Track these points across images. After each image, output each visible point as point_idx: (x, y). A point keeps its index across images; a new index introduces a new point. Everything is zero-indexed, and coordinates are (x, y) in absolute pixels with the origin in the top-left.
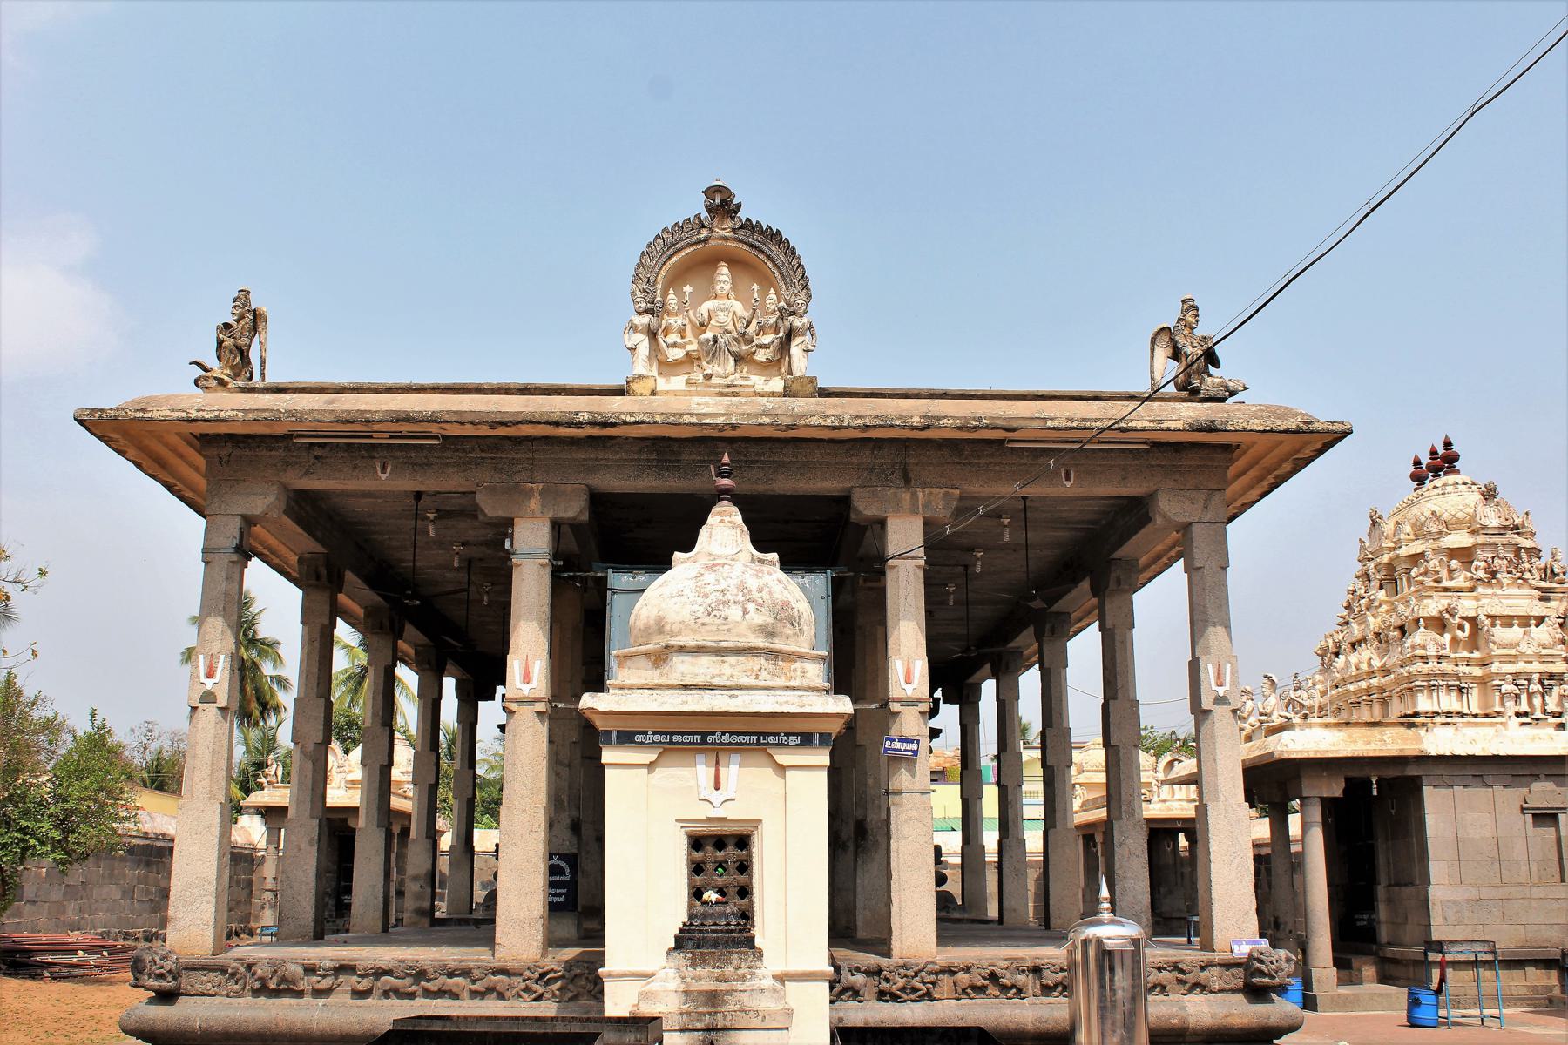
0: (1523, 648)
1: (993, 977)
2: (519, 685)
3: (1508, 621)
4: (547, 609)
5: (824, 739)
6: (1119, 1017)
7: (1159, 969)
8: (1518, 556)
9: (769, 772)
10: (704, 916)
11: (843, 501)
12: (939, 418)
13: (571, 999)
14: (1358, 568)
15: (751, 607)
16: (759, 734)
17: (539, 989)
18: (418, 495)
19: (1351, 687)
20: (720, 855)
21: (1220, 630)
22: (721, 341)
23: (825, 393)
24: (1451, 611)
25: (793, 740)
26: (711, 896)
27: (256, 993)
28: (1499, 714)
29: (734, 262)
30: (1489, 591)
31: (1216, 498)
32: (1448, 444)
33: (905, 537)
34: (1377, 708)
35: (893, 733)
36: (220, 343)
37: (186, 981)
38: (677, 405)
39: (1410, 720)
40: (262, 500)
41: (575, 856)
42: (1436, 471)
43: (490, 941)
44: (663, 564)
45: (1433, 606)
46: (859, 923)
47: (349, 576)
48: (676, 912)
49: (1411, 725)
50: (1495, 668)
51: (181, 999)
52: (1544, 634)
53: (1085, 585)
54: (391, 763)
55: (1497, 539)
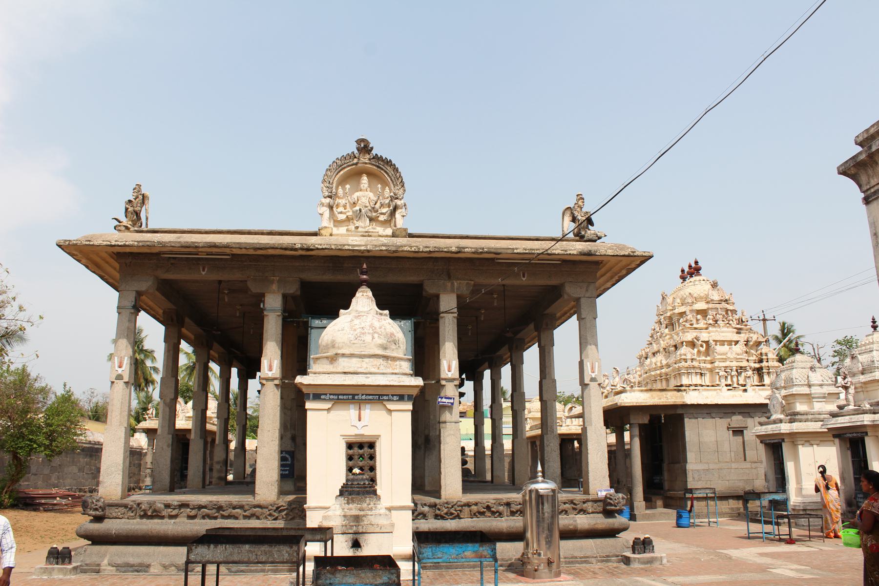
0: (729, 355)
1: (488, 508)
2: (267, 372)
3: (722, 343)
4: (280, 336)
5: (410, 397)
6: (546, 525)
7: (565, 503)
8: (727, 313)
9: (384, 412)
10: (353, 480)
11: (419, 286)
12: (464, 248)
13: (291, 519)
14: (656, 319)
15: (376, 335)
16: (379, 395)
17: (276, 514)
18: (220, 282)
19: (653, 373)
20: (361, 451)
21: (593, 347)
22: (363, 211)
23: (411, 236)
24: (697, 338)
25: (395, 398)
26: (356, 471)
27: (142, 517)
28: (718, 385)
29: (370, 174)
30: (714, 329)
31: (592, 287)
32: (696, 263)
33: (448, 303)
34: (664, 382)
35: (442, 395)
36: (127, 209)
37: (108, 512)
38: (341, 241)
39: (679, 388)
40: (145, 284)
41: (293, 452)
42: (691, 275)
43: (253, 492)
44: (336, 315)
45: (689, 336)
46: (426, 483)
47: (187, 320)
48: (340, 478)
49: (679, 391)
50: (716, 364)
51: (106, 520)
52: (739, 348)
53: (532, 326)
54: (206, 408)
55: (718, 306)
